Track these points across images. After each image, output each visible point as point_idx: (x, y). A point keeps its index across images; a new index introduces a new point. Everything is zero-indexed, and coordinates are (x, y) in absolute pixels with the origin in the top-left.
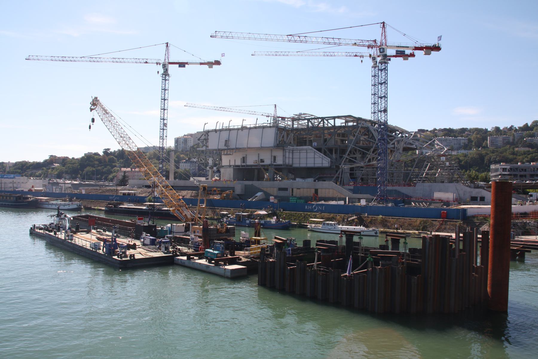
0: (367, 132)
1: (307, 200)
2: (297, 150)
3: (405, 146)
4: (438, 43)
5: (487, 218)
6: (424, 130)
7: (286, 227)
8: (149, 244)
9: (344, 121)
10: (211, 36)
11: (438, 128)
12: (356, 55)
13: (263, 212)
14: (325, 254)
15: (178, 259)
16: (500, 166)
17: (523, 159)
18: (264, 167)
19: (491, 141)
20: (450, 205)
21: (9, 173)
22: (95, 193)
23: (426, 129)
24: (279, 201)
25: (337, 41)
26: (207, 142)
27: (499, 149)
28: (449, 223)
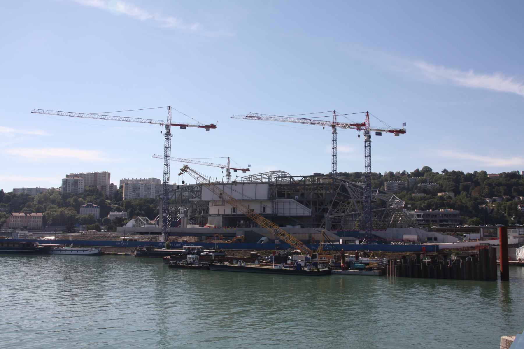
17: (421, 204)
19: (388, 186)
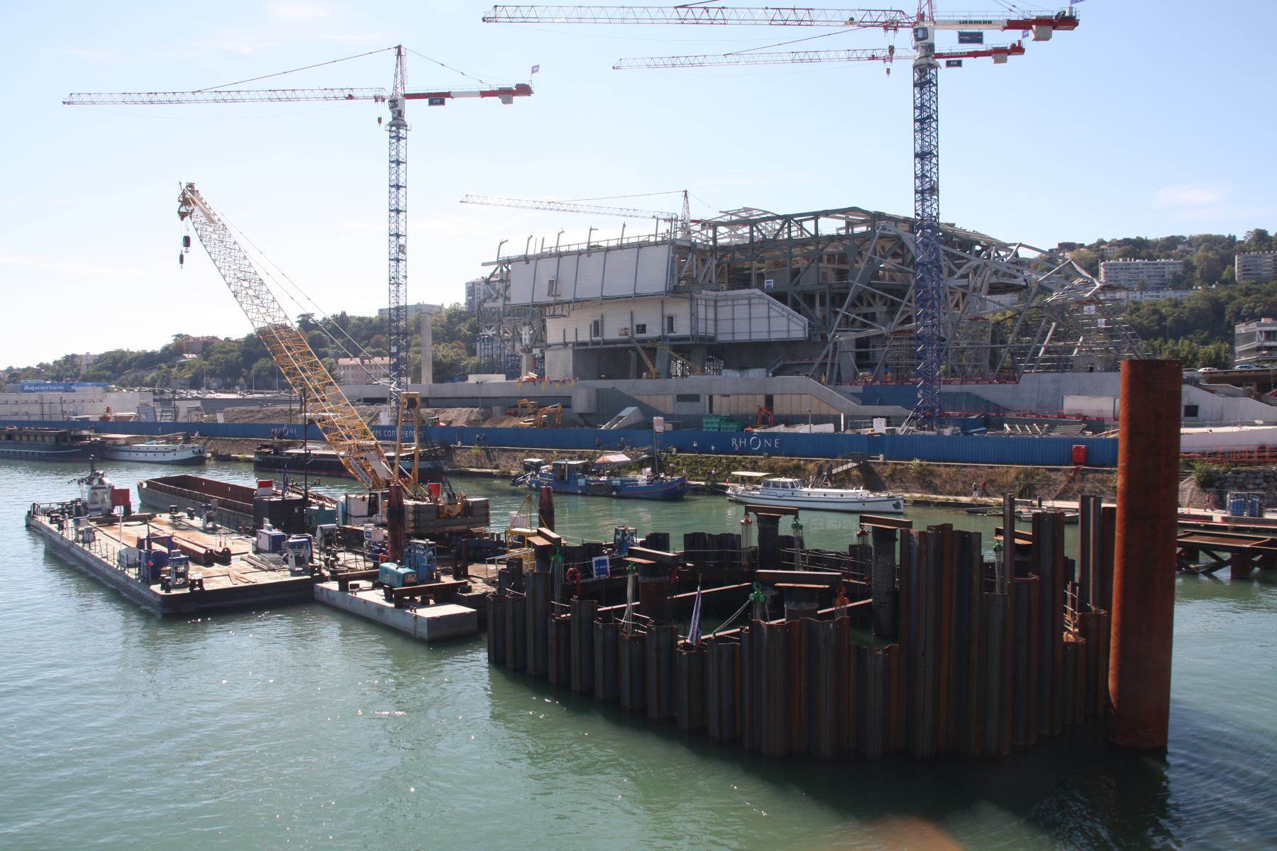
0: (898, 248)
1: (744, 422)
2: (727, 300)
3: (994, 280)
4: (1071, 8)
5: (1193, 461)
6: (1074, 244)
7: (675, 495)
8: (267, 549)
9: (842, 223)
10: (484, 20)
11: (1107, 239)
12: (873, 56)
13: (619, 458)
14: (647, 580)
15: (322, 588)
16: (1258, 326)
18: (643, 345)
20: (1106, 428)
21: (86, 379)
22: (247, 420)
23: (1078, 242)
24: (676, 427)
25: (801, 15)
26: (507, 287)
27: (1264, 285)
28: (1091, 476)
